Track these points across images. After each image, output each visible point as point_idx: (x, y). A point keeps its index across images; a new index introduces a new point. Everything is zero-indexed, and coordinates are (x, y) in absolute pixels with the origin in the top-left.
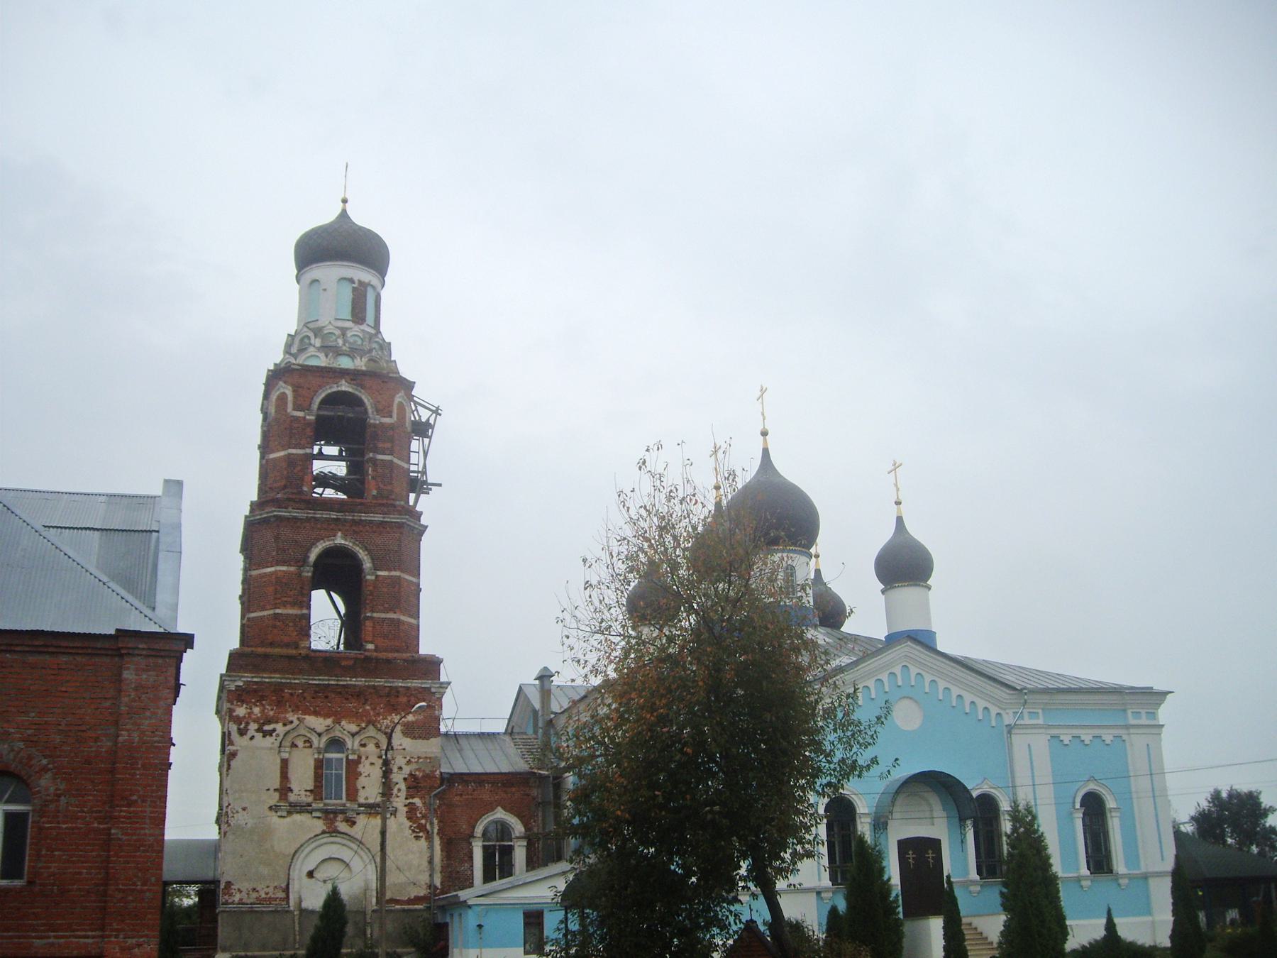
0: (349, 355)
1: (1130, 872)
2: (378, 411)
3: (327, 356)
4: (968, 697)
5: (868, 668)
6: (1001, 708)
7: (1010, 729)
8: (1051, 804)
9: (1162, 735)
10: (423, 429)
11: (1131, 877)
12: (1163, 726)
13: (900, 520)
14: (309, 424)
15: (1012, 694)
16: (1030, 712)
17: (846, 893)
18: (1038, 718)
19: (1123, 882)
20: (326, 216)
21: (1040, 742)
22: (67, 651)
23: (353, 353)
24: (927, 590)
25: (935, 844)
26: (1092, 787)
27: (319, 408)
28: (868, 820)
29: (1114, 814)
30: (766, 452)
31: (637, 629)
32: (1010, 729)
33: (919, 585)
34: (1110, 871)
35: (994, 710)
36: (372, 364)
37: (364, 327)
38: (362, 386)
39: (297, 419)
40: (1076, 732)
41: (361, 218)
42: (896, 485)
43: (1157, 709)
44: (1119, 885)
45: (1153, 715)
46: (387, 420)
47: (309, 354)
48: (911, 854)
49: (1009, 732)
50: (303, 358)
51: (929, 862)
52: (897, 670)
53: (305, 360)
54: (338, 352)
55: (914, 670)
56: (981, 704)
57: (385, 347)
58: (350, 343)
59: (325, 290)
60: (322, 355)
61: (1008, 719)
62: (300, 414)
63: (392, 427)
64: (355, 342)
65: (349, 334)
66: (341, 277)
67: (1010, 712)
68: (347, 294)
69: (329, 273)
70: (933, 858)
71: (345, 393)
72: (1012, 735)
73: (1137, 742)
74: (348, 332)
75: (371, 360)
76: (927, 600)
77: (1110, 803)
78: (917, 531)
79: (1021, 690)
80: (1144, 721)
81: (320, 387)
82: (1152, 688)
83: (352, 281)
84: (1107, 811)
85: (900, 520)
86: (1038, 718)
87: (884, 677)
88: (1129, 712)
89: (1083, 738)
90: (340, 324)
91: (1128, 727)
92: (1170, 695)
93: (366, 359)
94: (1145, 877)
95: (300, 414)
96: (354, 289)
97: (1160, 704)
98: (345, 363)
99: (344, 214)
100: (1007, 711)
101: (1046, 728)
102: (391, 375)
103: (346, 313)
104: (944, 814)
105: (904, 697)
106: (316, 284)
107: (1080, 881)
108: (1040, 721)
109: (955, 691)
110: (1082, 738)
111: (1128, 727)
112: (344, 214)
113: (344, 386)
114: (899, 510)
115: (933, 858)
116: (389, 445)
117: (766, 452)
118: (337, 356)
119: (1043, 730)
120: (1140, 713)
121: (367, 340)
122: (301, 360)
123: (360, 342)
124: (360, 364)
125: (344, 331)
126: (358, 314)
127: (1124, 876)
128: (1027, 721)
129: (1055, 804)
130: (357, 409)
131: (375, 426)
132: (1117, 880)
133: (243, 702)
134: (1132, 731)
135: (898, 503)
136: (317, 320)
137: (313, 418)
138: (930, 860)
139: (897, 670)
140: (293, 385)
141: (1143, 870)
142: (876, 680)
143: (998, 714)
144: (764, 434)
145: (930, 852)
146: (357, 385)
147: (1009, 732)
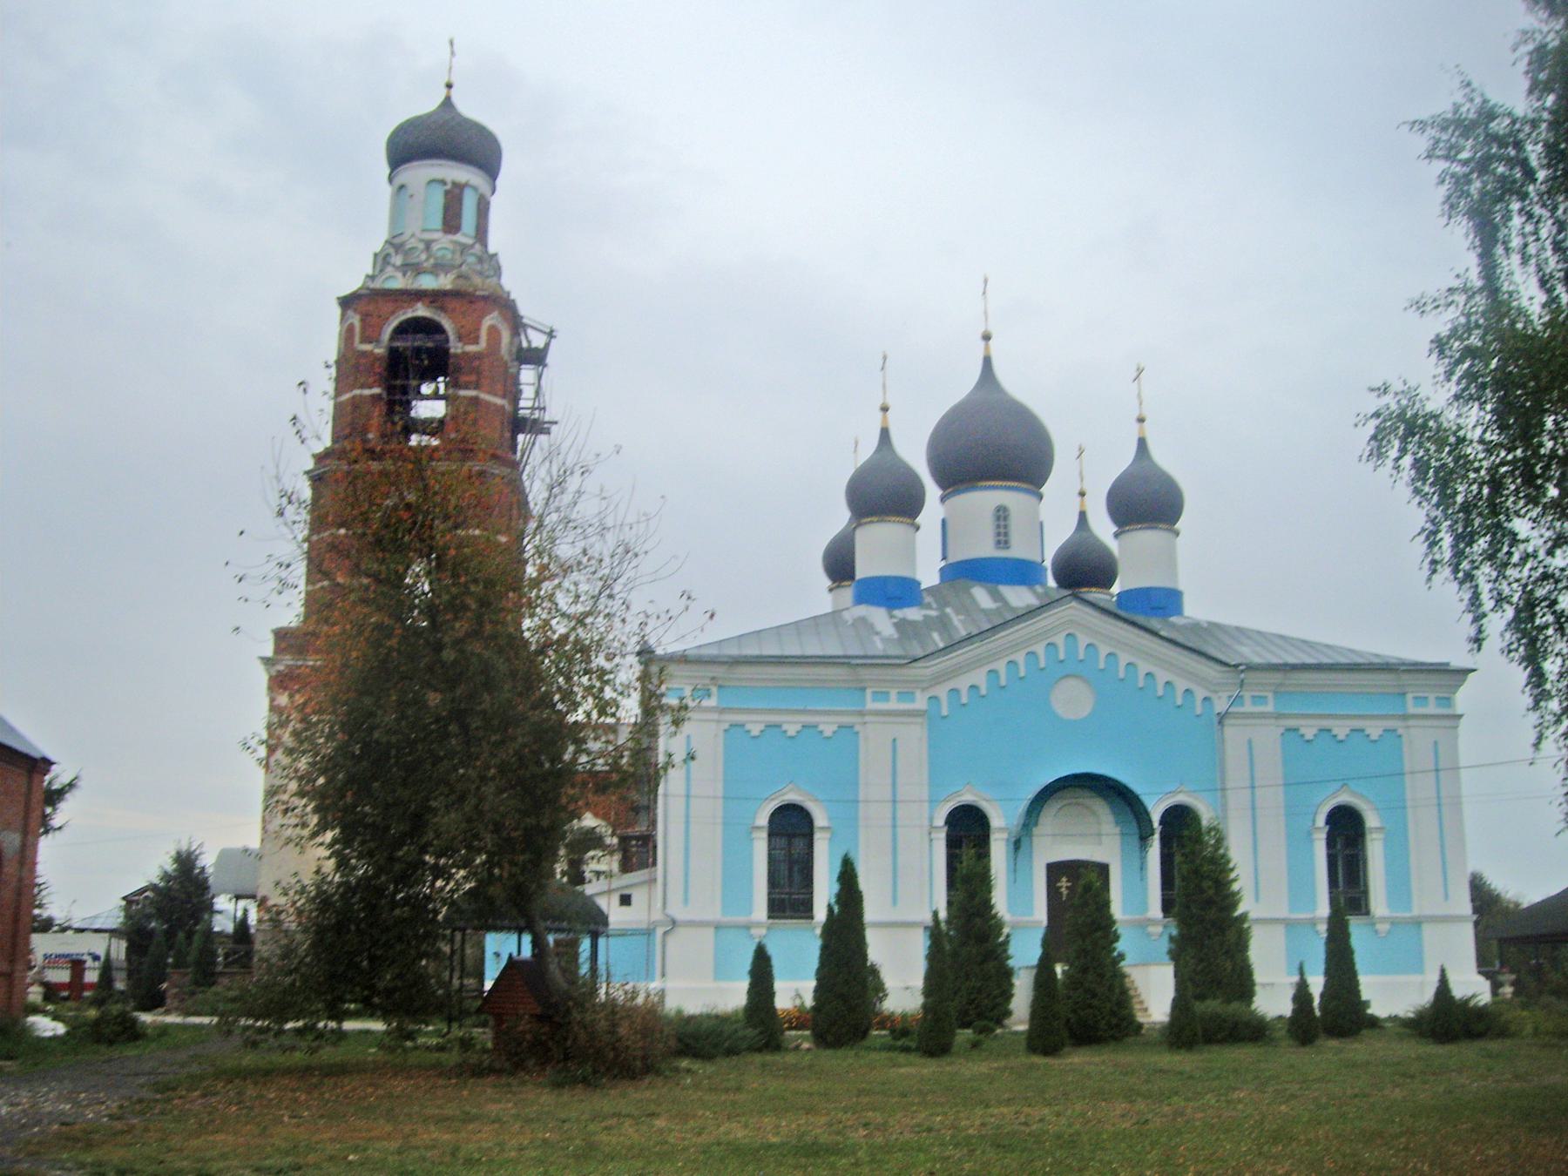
0: (431, 273)
1: (1395, 915)
2: (460, 338)
3: (404, 275)
4: (1162, 676)
5: (1011, 638)
6: (1211, 691)
7: (1222, 718)
8: (715, 797)
9: (1460, 728)
10: (536, 358)
11: (1394, 922)
12: (1460, 716)
13: (1142, 444)
14: (377, 358)
15: (1224, 672)
16: (1253, 697)
17: (1175, 932)
18: (1266, 703)
19: (1383, 928)
20: (427, 104)
21: (1268, 737)
22: (831, 660)
23: (438, 268)
24: (912, 530)
25: (1103, 870)
26: (1344, 798)
27: (392, 338)
28: (1005, 836)
29: (1374, 836)
30: (987, 362)
31: (485, 583)
32: (1222, 718)
33: (1156, 528)
34: (1367, 913)
35: (1200, 693)
36: (461, 282)
37: (459, 237)
38: (443, 309)
39: (364, 354)
40: (1326, 723)
41: (468, 108)
42: (1139, 396)
43: (1454, 693)
44: (1376, 932)
45: (1447, 701)
46: (471, 348)
47: (387, 275)
48: (1064, 883)
49: (1220, 722)
50: (381, 279)
51: (1061, 894)
52: (1059, 640)
53: (383, 282)
54: (418, 270)
55: (1083, 640)
56: (1181, 685)
57: (491, 263)
58: (436, 259)
59: (411, 196)
60: (399, 275)
61: (1221, 705)
62: (367, 347)
63: (478, 356)
64: (443, 257)
65: (435, 247)
66: (428, 180)
67: (1225, 695)
68: (438, 199)
69: (420, 173)
70: (1067, 888)
71: (424, 319)
72: (1226, 728)
73: (1418, 742)
74: (433, 244)
75: (459, 277)
76: (913, 542)
77: (1371, 821)
78: (1164, 458)
79: (1236, 666)
80: (1432, 709)
81: (393, 313)
82: (1448, 664)
83: (443, 182)
84: (1367, 832)
85: (1142, 444)
86: (1266, 703)
87: (1040, 649)
88: (1410, 696)
89: (1303, 731)
90: (427, 236)
91: (1405, 717)
92: (1471, 675)
93: (453, 277)
94: (1418, 922)
95: (367, 347)
96: (447, 193)
97: (1460, 686)
98: (427, 282)
99: (447, 103)
100: (1220, 694)
101: (1276, 718)
102: (478, 293)
103: (436, 220)
104: (1118, 830)
105: (1067, 676)
106: (403, 190)
107: (1315, 924)
108: (1269, 708)
109: (1143, 667)
110: (1334, 732)
111: (1405, 717)
112: (447, 103)
113: (421, 311)
114: (1141, 430)
115: (1067, 888)
116: (473, 378)
117: (987, 362)
118: (416, 276)
119: (1273, 721)
120: (1426, 698)
121: (458, 253)
122: (377, 284)
123: (449, 256)
124: (445, 282)
125: (428, 245)
126: (451, 222)
127: (1383, 919)
128: (1248, 708)
129: (724, 798)
130: (438, 337)
131: (456, 355)
132: (1373, 924)
133: (285, 689)
134: (1411, 722)
135: (1141, 420)
136: (401, 234)
137: (380, 351)
138: (1063, 889)
139: (1059, 640)
140: (361, 313)
141: (1416, 912)
142: (1027, 654)
143: (1206, 699)
144: (987, 337)
145: (1064, 879)
146: (436, 308)
147: (1220, 722)
